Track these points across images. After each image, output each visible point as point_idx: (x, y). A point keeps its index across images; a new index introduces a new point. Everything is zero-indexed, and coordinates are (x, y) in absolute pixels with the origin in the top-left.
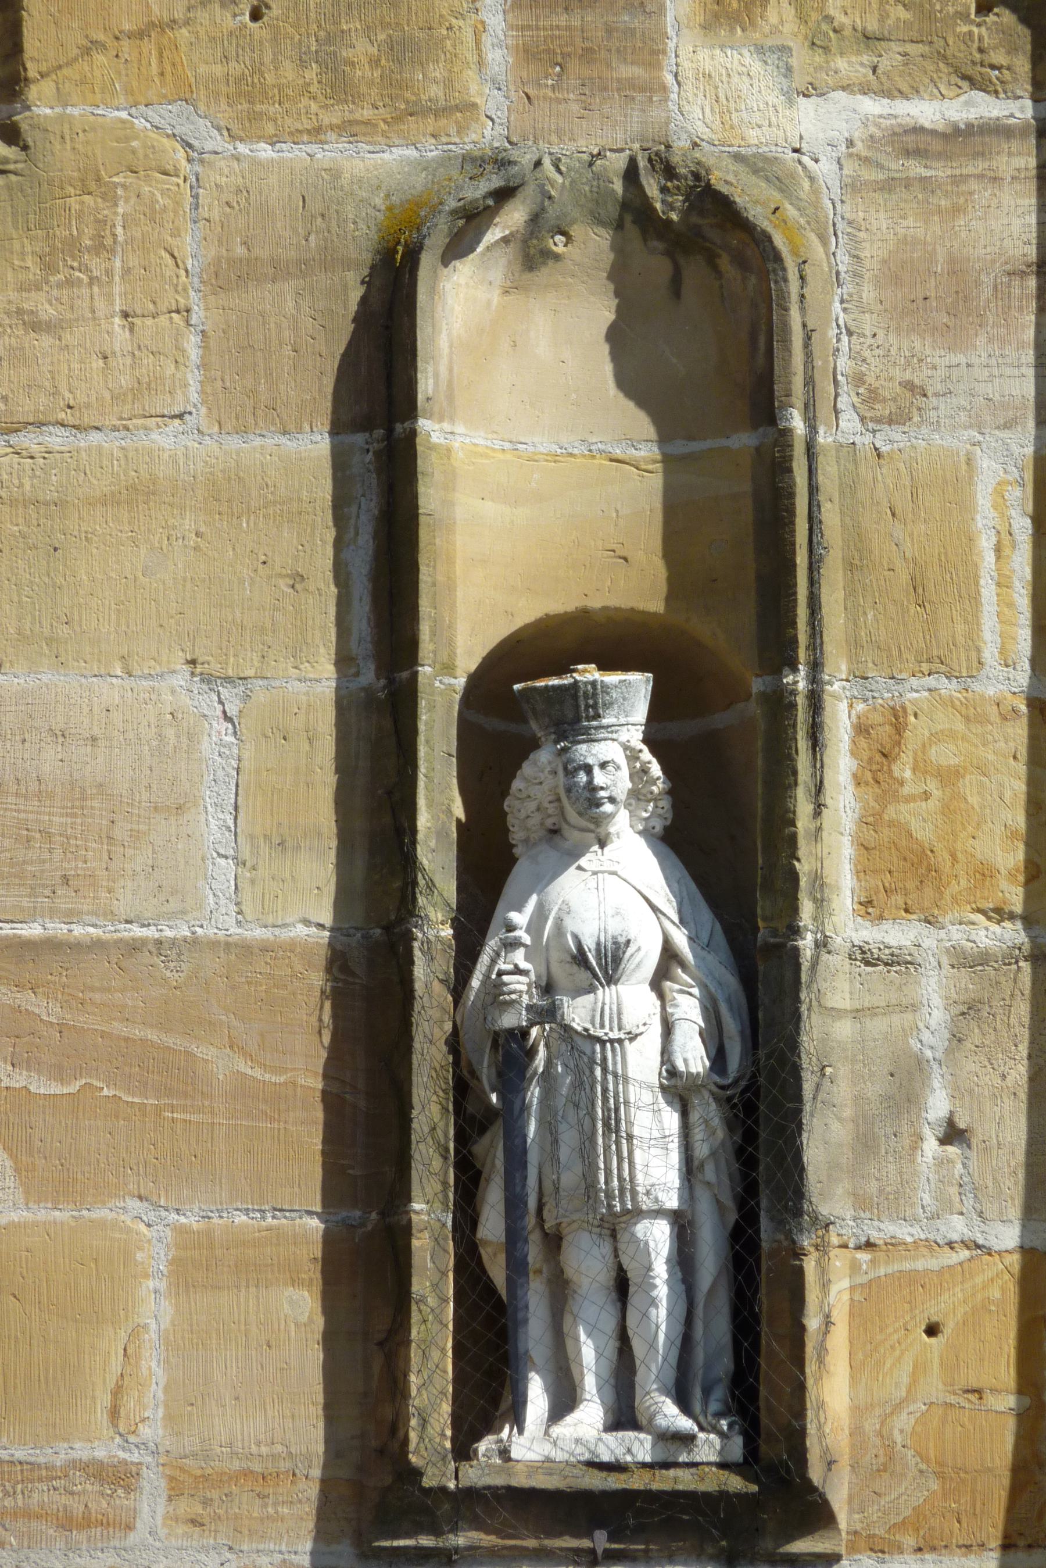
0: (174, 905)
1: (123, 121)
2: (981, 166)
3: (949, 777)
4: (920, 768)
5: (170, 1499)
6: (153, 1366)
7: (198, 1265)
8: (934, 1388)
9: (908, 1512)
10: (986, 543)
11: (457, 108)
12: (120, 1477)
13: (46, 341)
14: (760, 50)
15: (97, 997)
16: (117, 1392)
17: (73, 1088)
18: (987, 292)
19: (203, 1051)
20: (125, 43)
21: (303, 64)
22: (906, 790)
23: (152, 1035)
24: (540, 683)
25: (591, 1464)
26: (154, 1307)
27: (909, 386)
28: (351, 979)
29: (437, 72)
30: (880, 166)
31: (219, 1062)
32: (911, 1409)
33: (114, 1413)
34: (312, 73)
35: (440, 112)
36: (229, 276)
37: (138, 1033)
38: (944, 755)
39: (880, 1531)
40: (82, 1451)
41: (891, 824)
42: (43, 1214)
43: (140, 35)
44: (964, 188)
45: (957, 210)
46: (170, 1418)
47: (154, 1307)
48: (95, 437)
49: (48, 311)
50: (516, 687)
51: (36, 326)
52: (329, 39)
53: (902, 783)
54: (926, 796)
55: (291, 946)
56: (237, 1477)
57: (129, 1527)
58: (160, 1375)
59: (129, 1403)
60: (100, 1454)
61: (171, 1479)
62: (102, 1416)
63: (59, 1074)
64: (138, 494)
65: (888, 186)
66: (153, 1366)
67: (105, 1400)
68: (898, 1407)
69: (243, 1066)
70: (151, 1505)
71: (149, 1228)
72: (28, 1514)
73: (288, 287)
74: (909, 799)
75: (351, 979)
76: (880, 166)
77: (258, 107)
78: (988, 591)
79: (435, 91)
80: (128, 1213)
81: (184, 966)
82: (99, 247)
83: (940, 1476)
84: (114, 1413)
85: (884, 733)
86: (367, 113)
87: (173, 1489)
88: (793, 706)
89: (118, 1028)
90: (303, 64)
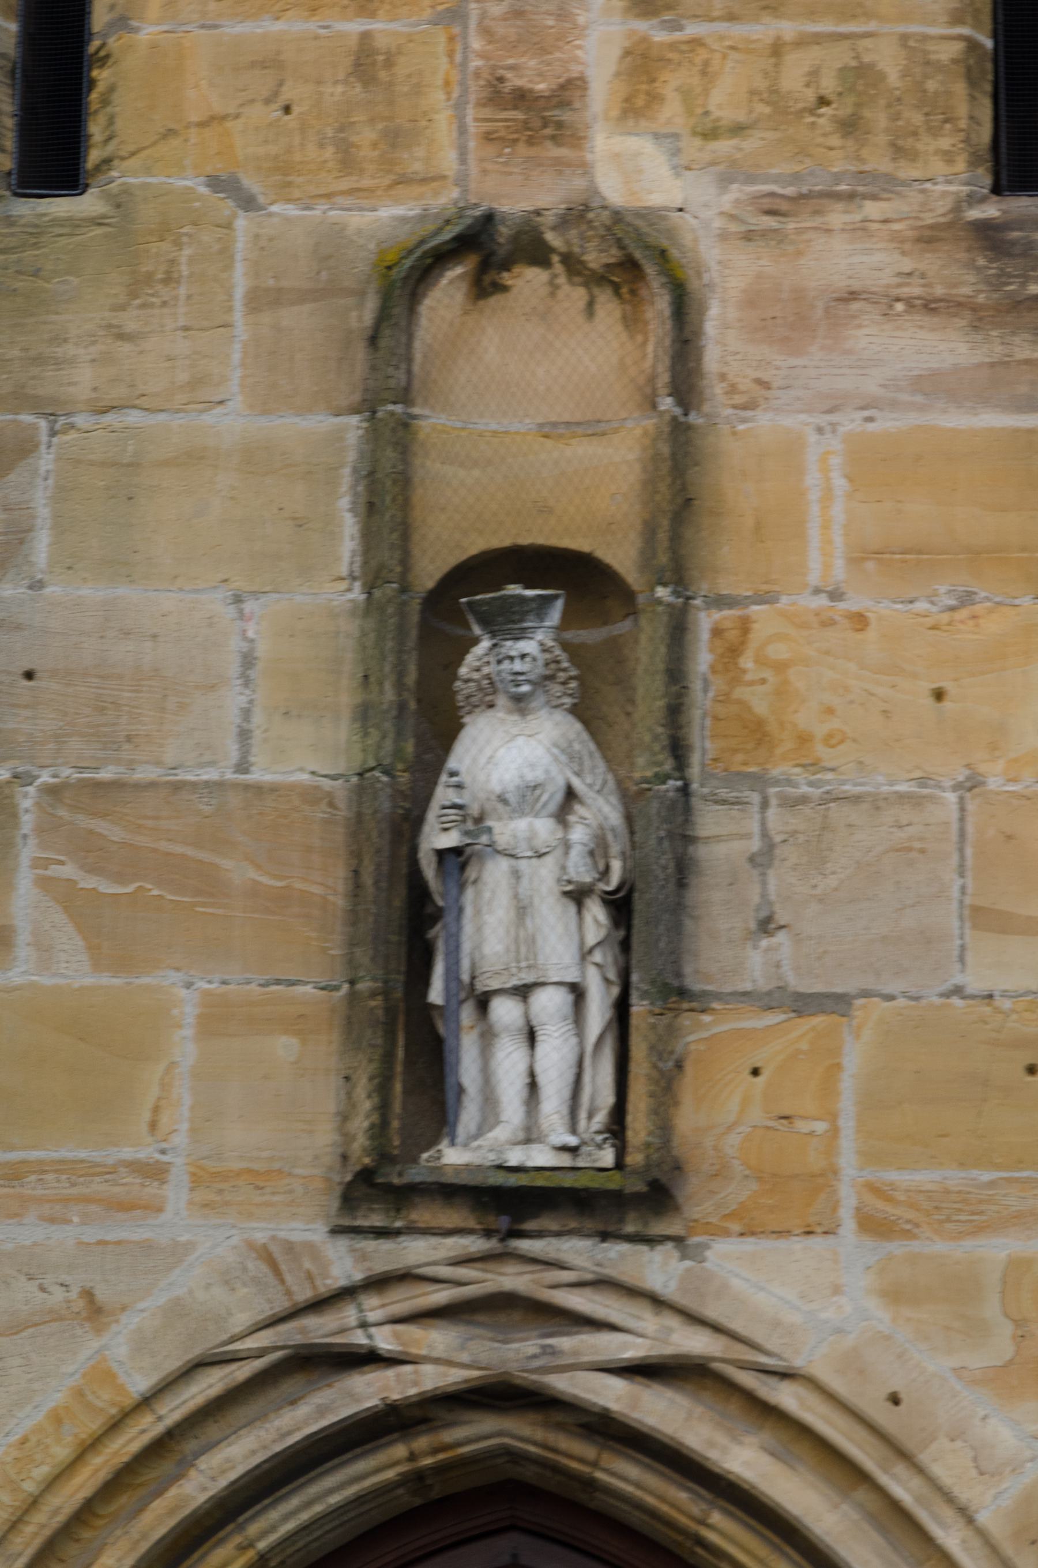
0: (206, 758)
1: (190, 188)
2: (817, 221)
3: (781, 667)
4: (761, 661)
5: (192, 1189)
6: (184, 1094)
7: (215, 1019)
8: (757, 1115)
9: (734, 1207)
10: (814, 495)
11: (433, 179)
12: (156, 1172)
13: (126, 348)
14: (657, 136)
15: (150, 823)
16: (156, 1110)
17: (130, 889)
18: (819, 313)
19: (226, 863)
20: (193, 130)
21: (321, 146)
22: (748, 677)
23: (190, 851)
24: (478, 597)
25: (500, 1167)
26: (184, 1047)
27: (759, 382)
28: (335, 812)
29: (420, 152)
30: (743, 222)
31: (238, 871)
32: (738, 1131)
33: (153, 1126)
34: (329, 152)
35: (424, 181)
36: (260, 300)
37: (179, 849)
38: (779, 651)
39: (714, 1220)
40: (127, 1153)
41: (739, 702)
42: (106, 980)
43: (202, 125)
44: (805, 237)
45: (799, 253)
46: (193, 1131)
47: (184, 1047)
48: (162, 417)
49: (131, 326)
50: (463, 600)
51: (122, 337)
52: (341, 129)
53: (744, 671)
54: (763, 681)
55: (292, 787)
56: (239, 1174)
57: (160, 1210)
58: (187, 1100)
59: (164, 1120)
60: (142, 1155)
61: (193, 1174)
62: (144, 1128)
63: (120, 878)
64: (194, 457)
65: (748, 236)
66: (184, 1094)
67: (147, 1116)
68: (730, 1128)
69: (252, 874)
70: (176, 1194)
71: (182, 992)
72: (87, 1200)
73: (307, 307)
74: (751, 683)
75: (335, 812)
76: (743, 222)
77: (290, 178)
78: (814, 533)
79: (418, 167)
80: (169, 979)
81: (213, 801)
82: (169, 280)
83: (759, 1179)
84: (153, 1126)
85: (733, 635)
86: (366, 182)
87: (193, 1182)
88: (499, 590)
89: (164, 846)
90: (321, 146)
